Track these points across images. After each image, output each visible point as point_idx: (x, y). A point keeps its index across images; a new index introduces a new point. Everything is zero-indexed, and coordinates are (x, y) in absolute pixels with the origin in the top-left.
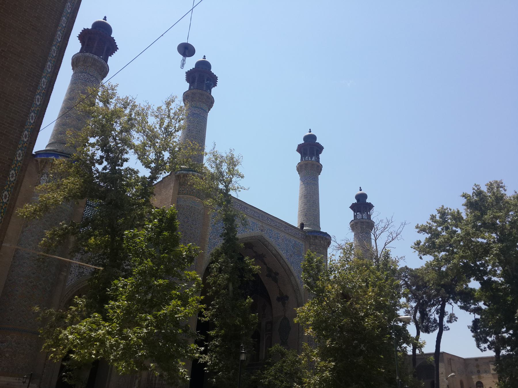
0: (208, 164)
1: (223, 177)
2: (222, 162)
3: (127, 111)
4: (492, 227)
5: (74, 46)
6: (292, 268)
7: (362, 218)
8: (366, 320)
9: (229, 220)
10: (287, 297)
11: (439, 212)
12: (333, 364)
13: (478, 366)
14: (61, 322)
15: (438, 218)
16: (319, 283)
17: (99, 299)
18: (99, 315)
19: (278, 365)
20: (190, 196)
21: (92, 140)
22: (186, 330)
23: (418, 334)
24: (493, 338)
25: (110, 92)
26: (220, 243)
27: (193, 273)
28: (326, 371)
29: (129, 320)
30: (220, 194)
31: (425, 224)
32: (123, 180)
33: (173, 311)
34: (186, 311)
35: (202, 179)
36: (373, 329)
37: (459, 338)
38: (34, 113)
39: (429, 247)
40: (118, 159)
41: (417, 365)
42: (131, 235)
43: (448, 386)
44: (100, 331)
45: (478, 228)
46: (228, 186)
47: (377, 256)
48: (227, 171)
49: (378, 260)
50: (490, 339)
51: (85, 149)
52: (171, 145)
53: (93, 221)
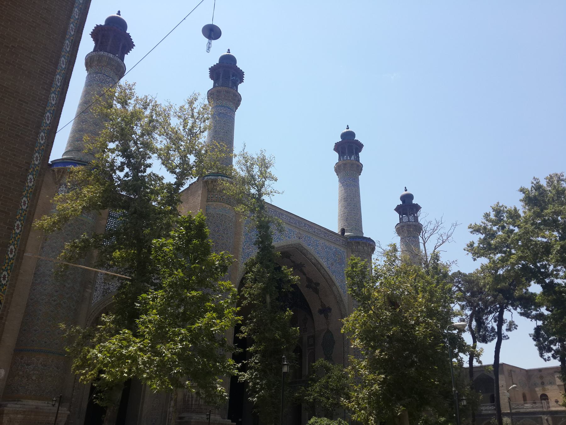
0: (238, 168)
1: (254, 181)
2: (252, 164)
3: (147, 112)
4: (552, 224)
5: (87, 45)
6: (334, 278)
7: (409, 221)
8: (417, 329)
9: (263, 227)
10: (329, 309)
11: (494, 210)
12: (383, 376)
13: (541, 377)
14: (87, 340)
15: (492, 216)
16: (364, 290)
17: (128, 316)
18: (129, 332)
19: (323, 381)
20: (220, 203)
21: (111, 145)
22: (223, 344)
23: (475, 342)
24: (557, 346)
25: (127, 91)
26: (254, 252)
27: (227, 284)
28: (375, 384)
29: (160, 336)
30: (252, 199)
31: (479, 223)
32: (148, 188)
33: (208, 324)
34: (222, 323)
35: (232, 184)
36: (425, 337)
37: (520, 347)
38: (50, 113)
39: (484, 248)
40: (140, 164)
41: (474, 378)
42: (159, 244)
43: (509, 398)
44: (131, 347)
45: (538, 226)
46: (261, 190)
47: (427, 261)
48: (259, 174)
49: (427, 266)
50: (554, 348)
51: (104, 155)
52: (197, 147)
53: (117, 233)
